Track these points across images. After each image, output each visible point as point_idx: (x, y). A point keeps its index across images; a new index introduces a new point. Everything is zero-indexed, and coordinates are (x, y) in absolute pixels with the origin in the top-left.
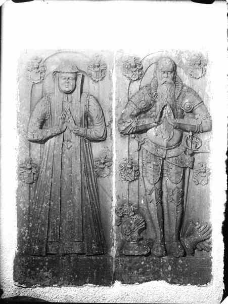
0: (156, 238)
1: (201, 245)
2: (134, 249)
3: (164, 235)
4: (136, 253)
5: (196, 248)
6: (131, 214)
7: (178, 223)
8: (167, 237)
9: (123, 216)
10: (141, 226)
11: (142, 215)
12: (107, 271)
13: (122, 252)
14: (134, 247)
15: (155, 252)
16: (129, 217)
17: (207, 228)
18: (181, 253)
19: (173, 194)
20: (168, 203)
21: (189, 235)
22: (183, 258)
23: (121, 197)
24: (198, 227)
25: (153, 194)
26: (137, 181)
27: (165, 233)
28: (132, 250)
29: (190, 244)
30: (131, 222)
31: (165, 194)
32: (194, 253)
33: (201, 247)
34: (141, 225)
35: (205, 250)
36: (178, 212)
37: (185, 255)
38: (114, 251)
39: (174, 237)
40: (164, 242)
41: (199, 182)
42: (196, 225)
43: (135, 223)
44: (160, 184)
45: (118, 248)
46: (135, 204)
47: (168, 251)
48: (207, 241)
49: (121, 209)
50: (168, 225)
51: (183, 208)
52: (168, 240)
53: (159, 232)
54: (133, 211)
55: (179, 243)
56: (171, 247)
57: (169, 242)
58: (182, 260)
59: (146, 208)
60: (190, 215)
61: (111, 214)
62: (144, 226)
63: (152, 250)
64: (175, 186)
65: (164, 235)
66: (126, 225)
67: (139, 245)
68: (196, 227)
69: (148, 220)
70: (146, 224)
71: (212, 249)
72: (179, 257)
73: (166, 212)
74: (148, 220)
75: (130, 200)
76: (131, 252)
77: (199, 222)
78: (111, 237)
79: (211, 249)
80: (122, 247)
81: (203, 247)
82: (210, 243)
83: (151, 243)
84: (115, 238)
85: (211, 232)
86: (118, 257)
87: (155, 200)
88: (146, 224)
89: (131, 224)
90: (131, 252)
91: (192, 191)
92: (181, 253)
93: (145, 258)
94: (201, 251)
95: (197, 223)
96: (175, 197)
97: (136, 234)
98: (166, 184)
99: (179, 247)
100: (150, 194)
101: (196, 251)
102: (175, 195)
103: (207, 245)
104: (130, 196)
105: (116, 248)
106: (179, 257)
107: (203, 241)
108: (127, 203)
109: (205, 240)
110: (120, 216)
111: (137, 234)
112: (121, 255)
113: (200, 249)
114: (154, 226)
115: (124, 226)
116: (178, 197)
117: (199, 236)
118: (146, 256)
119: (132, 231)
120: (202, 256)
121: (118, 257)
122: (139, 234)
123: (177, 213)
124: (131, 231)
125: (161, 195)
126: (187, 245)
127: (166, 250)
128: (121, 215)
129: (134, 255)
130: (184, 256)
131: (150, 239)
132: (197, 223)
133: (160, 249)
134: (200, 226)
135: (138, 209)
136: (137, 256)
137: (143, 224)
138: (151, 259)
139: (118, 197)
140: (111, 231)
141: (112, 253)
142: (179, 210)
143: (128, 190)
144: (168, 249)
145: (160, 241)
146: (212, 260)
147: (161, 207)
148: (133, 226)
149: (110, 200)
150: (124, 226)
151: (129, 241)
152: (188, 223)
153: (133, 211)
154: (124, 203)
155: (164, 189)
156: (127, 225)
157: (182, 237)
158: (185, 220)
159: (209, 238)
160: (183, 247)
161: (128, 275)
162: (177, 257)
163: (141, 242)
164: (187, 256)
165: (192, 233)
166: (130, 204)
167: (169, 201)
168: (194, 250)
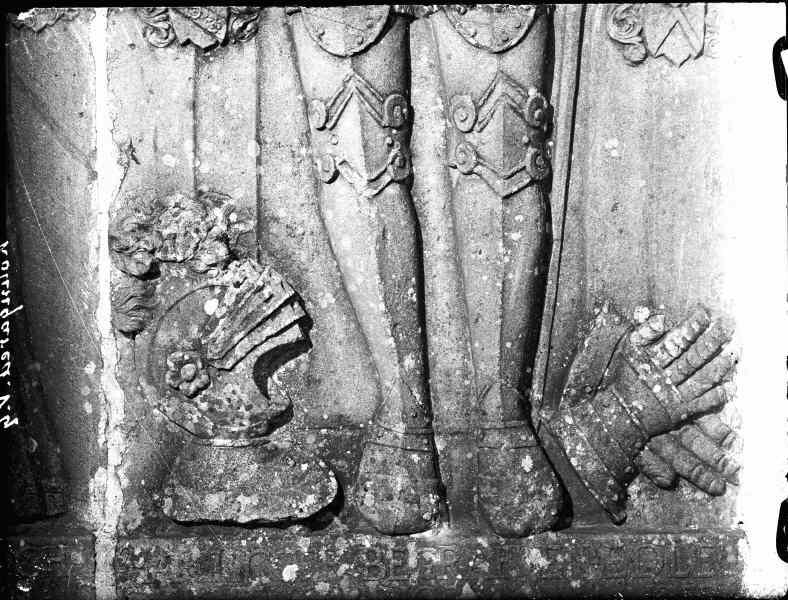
0: (379, 412)
1: (668, 449)
2: (235, 488)
3: (426, 389)
4: (246, 509)
5: (637, 471)
6: (206, 259)
7: (519, 317)
8: (446, 406)
9: (152, 273)
10: (267, 339)
11: (283, 264)
12: (683, 175)
13: (157, 506)
14: (232, 474)
15: (369, 499)
16: (195, 275)
17: (706, 345)
18: (540, 507)
19: (478, 124)
20: (451, 191)
21: (591, 388)
22: (552, 536)
23: (144, 153)
24: (646, 333)
25: (350, 125)
26: (250, 49)
27: (437, 379)
28: (219, 489)
29: (600, 441)
30: (211, 307)
31: (429, 134)
32: (623, 502)
33: (668, 462)
34: (269, 330)
35: (695, 484)
36: (515, 236)
37: (563, 516)
38: (107, 500)
39: (494, 401)
40: (430, 436)
41: (653, 47)
42: (634, 327)
43: (232, 313)
44: (398, 63)
45: (131, 476)
46: (241, 194)
47: (454, 490)
48: (710, 423)
49: (143, 228)
50: (453, 329)
51: (546, 216)
52: (456, 422)
53: (394, 370)
54: (223, 239)
55: (525, 437)
56: (477, 468)
57: (465, 437)
58: (546, 551)
59: (313, 223)
60: (605, 251)
61: (84, 261)
62: (294, 334)
63: (350, 490)
64: (489, 66)
65: (426, 389)
66: (175, 334)
67: (270, 455)
68: (634, 338)
69: (327, 300)
70: (306, 323)
71: (740, 475)
72: (528, 531)
73: (437, 248)
74: (327, 300)
75: (205, 169)
76: (213, 504)
77: (650, 304)
78: (88, 408)
79: (732, 478)
80: (169, 465)
81: (683, 465)
82: (722, 440)
83: (345, 445)
84: (117, 416)
85: (730, 369)
86: (131, 536)
87: (358, 161)
88: (306, 323)
89: (210, 323)
90: (213, 501)
91: (603, 105)
92: (537, 504)
93: (304, 544)
94: (674, 485)
95: (642, 314)
96: (490, 141)
97: (238, 387)
98: (437, 66)
99: (527, 463)
100: (329, 124)
101: (633, 488)
102: (494, 127)
103: (703, 447)
104: (206, 146)
105: (125, 482)
106: (528, 531)
107: (679, 424)
108: (188, 186)
109: (693, 418)
110: (135, 270)
111: (251, 384)
112: (154, 524)
113: (665, 478)
114: (360, 337)
115: (163, 338)
116: (509, 140)
117: (656, 387)
118: (315, 523)
119: (213, 368)
120: (675, 520)
121: (131, 536)
122: (260, 379)
123: (508, 244)
124: (207, 364)
125: (405, 128)
126: (579, 452)
127: (441, 491)
128: (141, 262)
129: (231, 523)
130: (555, 528)
131: (340, 421)
132: (642, 314)
133: (399, 481)
134: (658, 325)
135: (261, 227)
136: (254, 525)
137: (289, 316)
138: (342, 546)
139: (129, 153)
140: (90, 369)
141: (94, 507)
142: (518, 228)
143: (194, 106)
144: (455, 481)
145: (400, 428)
146: (741, 543)
147: (400, 208)
148: (219, 334)
149: (82, 174)
150: (163, 338)
151: (201, 435)
152: (583, 317)
153: (223, 239)
154: (171, 192)
155: (425, 98)
156: (184, 325)
157: (541, 405)
158: (563, 294)
159: (717, 408)
160: (551, 461)
161: (656, 93)
162: (511, 535)
163: (281, 438)
164: (578, 525)
165: (613, 371)
166: (205, 199)
167: (455, 174)
168: (624, 480)
